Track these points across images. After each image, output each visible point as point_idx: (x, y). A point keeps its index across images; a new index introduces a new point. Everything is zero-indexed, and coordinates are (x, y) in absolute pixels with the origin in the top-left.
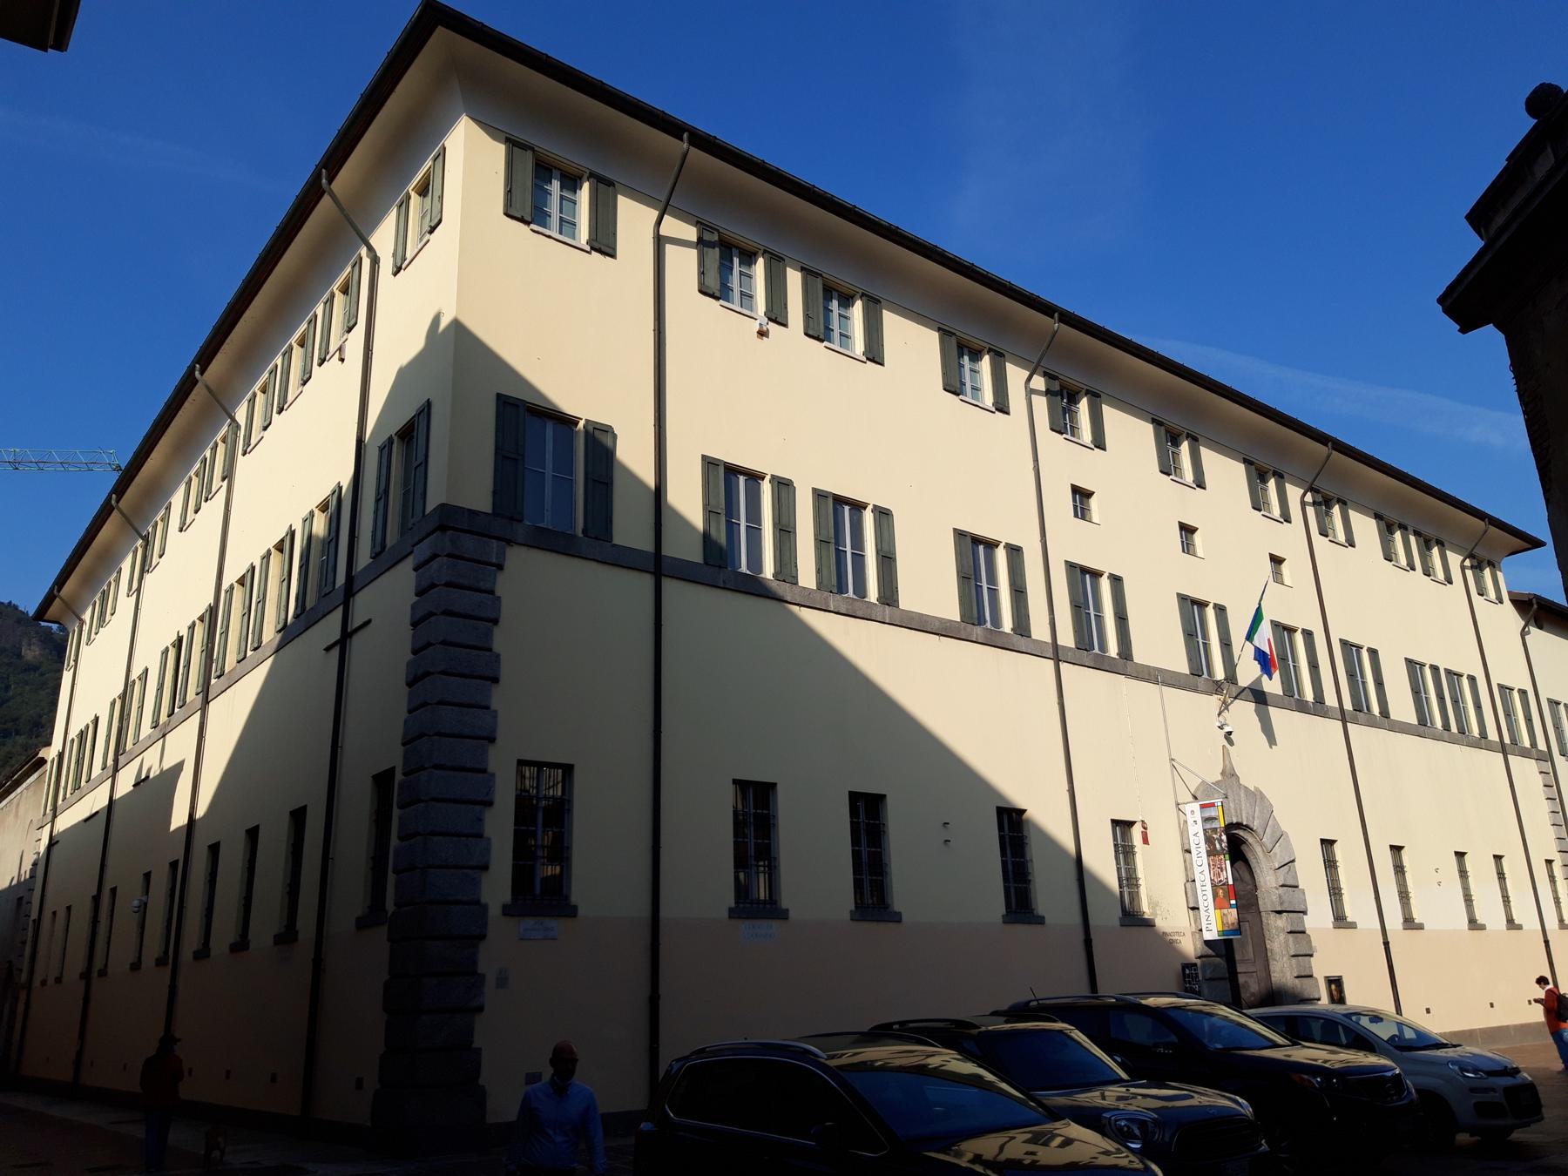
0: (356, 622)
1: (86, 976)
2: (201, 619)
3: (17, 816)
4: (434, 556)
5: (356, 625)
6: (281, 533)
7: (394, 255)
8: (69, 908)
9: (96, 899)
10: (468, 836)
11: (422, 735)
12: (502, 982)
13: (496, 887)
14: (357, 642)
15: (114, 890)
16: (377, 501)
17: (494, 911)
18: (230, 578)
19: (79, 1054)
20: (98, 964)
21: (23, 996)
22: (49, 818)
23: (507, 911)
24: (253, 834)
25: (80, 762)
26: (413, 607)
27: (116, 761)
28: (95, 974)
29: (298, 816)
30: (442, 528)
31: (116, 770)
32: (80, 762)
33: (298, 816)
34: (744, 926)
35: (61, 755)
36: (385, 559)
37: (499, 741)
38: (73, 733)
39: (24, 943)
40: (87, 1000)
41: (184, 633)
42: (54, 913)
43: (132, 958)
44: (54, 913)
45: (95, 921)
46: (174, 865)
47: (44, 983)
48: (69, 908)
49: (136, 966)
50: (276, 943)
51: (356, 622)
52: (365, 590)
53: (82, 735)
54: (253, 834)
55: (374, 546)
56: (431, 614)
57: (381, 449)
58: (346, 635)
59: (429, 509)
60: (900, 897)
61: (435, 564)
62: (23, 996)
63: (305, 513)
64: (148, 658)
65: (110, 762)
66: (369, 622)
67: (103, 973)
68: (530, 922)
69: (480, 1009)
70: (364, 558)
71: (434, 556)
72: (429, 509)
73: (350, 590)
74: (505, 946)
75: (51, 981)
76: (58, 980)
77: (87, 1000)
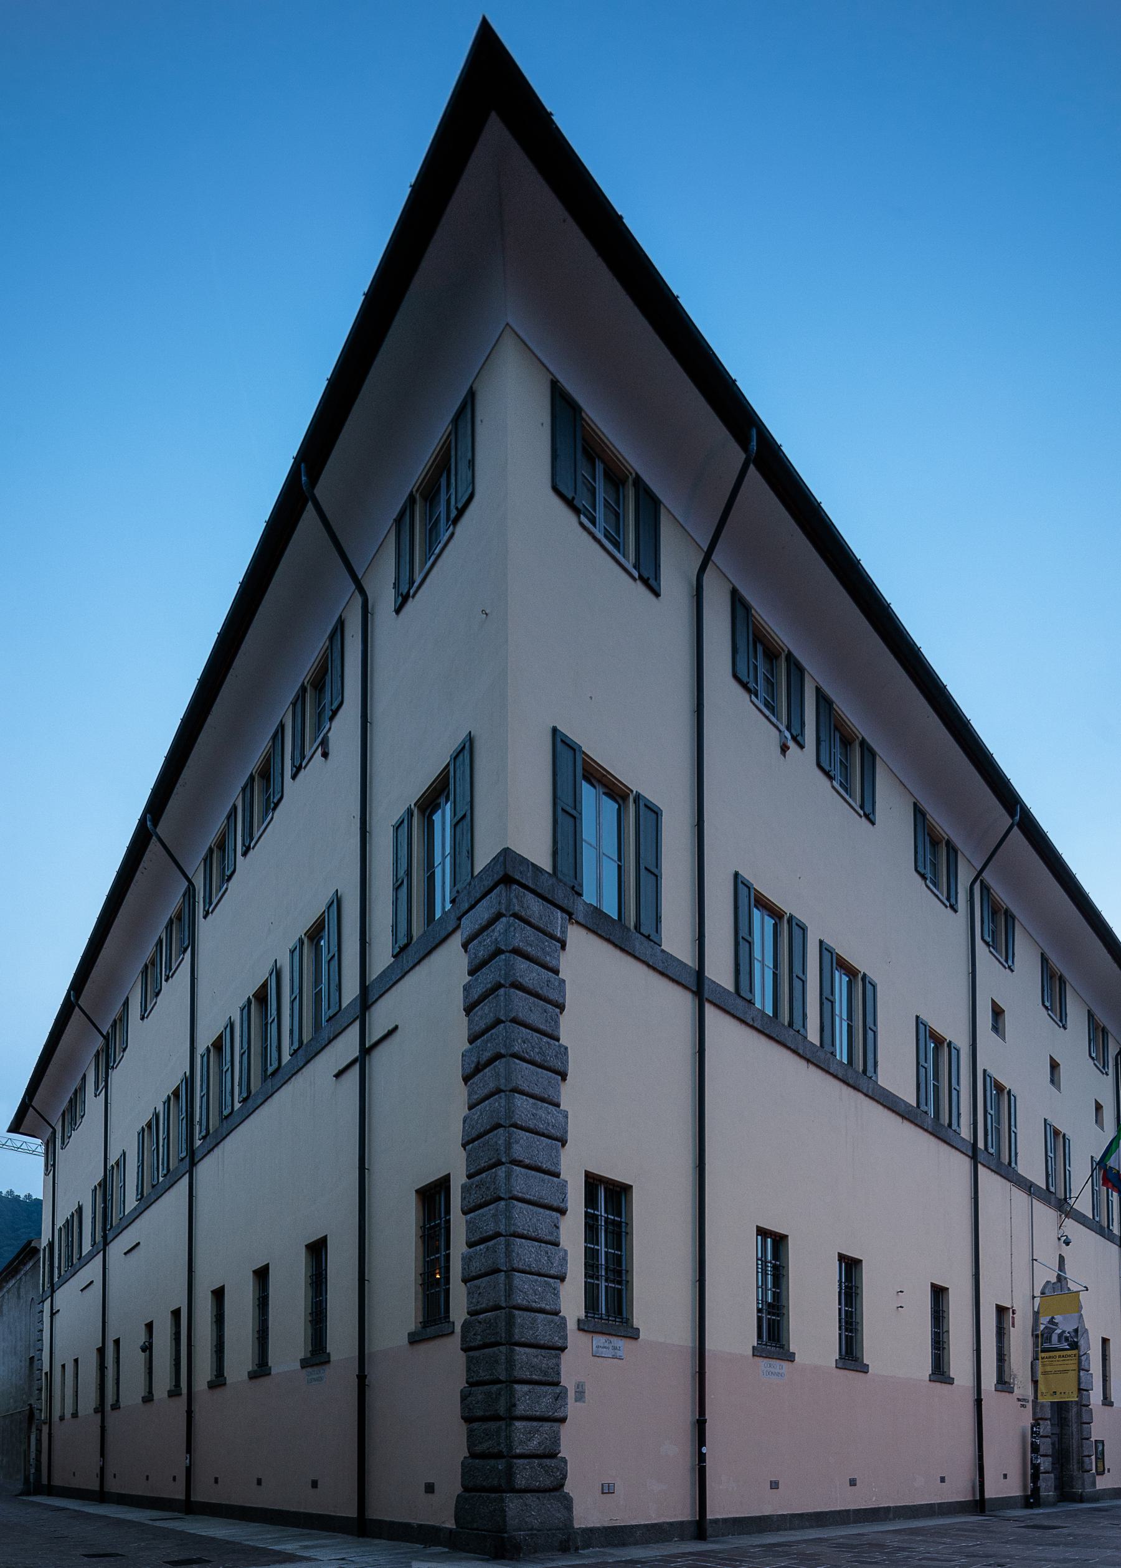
0: (376, 1032)
1: (100, 1409)
2: (100, 1184)
3: (19, 1297)
4: (499, 916)
5: (375, 1039)
6: (262, 974)
7: (396, 585)
8: (76, 1361)
9: (101, 1351)
10: (547, 1242)
11: (498, 1126)
12: (580, 1395)
13: (572, 1300)
14: (380, 1059)
15: (117, 1342)
16: (397, 889)
17: (572, 1325)
18: (202, 1045)
19: (102, 1469)
20: (110, 1399)
21: (45, 1429)
22: (48, 1293)
23: (582, 1327)
24: (262, 1275)
25: (69, 1245)
26: (467, 988)
27: (105, 1237)
28: (108, 1408)
29: (317, 1250)
30: (507, 880)
31: (106, 1243)
32: (69, 1245)
33: (317, 1250)
34: (763, 1363)
35: (51, 1245)
36: (410, 953)
37: (573, 1134)
38: (60, 1223)
39: (40, 1390)
40: (103, 1428)
41: (285, 963)
42: (63, 1366)
43: (142, 1392)
44: (63, 1366)
45: (102, 1367)
46: (176, 1313)
47: (62, 1418)
48: (76, 1361)
49: (148, 1399)
50: (303, 1367)
51: (376, 1032)
52: (206, 1159)
53: (68, 1224)
54: (262, 1275)
55: (395, 940)
56: (499, 986)
57: (397, 828)
58: (366, 1051)
59: (478, 870)
60: (870, 1352)
61: (500, 926)
62: (45, 1429)
63: (165, 1098)
64: (125, 1141)
65: (98, 1238)
66: (138, 1244)
67: (116, 1406)
68: (600, 1340)
69: (563, 1420)
70: (382, 958)
71: (499, 916)
72: (478, 870)
73: (366, 1001)
74: (582, 1360)
75: (68, 1415)
76: (75, 1415)
77: (103, 1428)
